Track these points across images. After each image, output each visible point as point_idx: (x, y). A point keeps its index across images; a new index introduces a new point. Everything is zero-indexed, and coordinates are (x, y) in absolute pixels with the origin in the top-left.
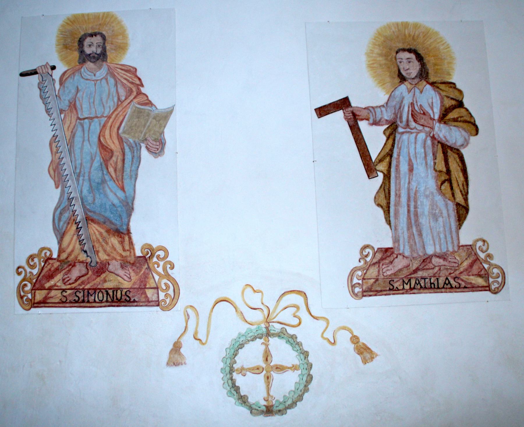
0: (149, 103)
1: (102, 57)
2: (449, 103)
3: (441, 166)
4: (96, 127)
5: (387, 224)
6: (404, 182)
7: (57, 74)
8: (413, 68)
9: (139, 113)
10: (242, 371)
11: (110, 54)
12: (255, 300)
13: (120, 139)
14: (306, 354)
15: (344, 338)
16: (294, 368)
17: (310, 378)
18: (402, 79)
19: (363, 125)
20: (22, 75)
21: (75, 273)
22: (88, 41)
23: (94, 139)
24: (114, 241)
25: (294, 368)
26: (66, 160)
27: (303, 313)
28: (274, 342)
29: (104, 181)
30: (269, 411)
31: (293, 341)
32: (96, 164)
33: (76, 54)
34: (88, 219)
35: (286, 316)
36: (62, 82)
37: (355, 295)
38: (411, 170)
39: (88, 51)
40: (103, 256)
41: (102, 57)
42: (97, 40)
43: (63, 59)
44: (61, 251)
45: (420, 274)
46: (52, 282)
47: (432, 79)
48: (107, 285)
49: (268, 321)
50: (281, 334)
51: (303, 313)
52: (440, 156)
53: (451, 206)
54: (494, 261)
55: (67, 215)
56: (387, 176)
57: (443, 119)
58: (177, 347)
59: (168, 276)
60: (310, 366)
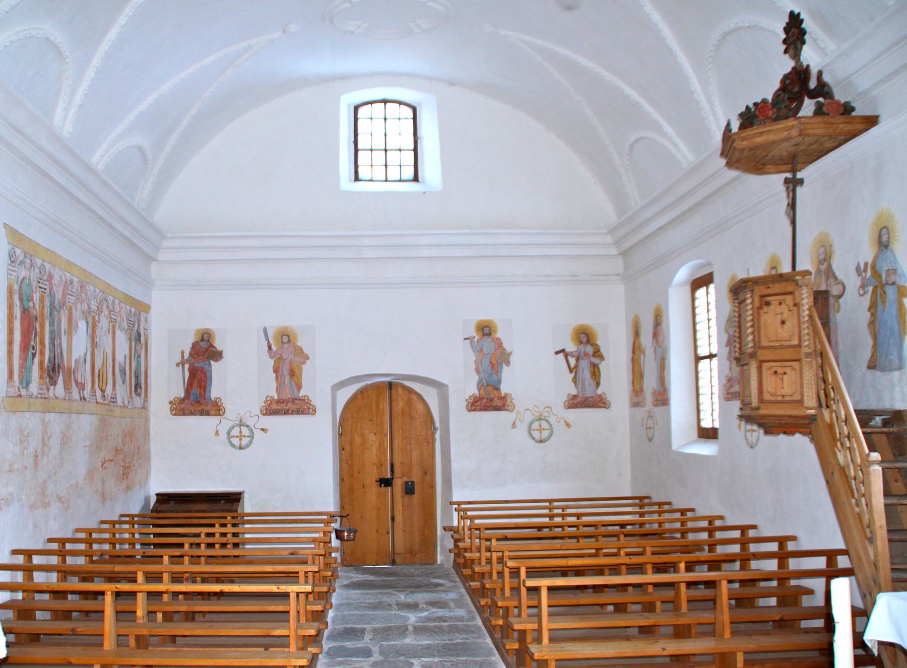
0: (504, 350)
1: (489, 334)
2: (595, 351)
3: (592, 370)
4: (489, 357)
5: (478, 388)
6: (581, 374)
7: (476, 339)
8: (585, 340)
9: (502, 353)
10: (533, 430)
11: (492, 334)
12: (537, 409)
13: (497, 361)
14: (551, 425)
15: (562, 421)
16: (548, 429)
17: (552, 432)
18: (582, 343)
19: (569, 358)
20: (465, 339)
21: (484, 401)
22: (485, 329)
23: (489, 361)
24: (496, 392)
25: (548, 429)
26: (480, 367)
27: (550, 413)
28: (542, 422)
29: (492, 374)
30: (541, 442)
31: (548, 421)
32: (490, 368)
33: (481, 334)
34: (488, 385)
35: (546, 414)
36: (477, 342)
37: (566, 409)
38: (583, 371)
39: (485, 332)
40: (492, 396)
41: (489, 334)
42: (488, 329)
43: (478, 334)
44: (479, 395)
45: (585, 402)
46: (477, 404)
47: (591, 343)
48: (494, 405)
49: (540, 415)
50: (544, 420)
51: (550, 413)
52: (592, 367)
53: (595, 382)
54: (608, 399)
55: (481, 384)
56: (576, 373)
57: (594, 355)
58: (514, 423)
59: (511, 402)
60: (552, 429)
